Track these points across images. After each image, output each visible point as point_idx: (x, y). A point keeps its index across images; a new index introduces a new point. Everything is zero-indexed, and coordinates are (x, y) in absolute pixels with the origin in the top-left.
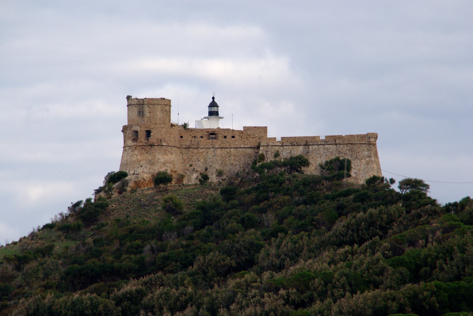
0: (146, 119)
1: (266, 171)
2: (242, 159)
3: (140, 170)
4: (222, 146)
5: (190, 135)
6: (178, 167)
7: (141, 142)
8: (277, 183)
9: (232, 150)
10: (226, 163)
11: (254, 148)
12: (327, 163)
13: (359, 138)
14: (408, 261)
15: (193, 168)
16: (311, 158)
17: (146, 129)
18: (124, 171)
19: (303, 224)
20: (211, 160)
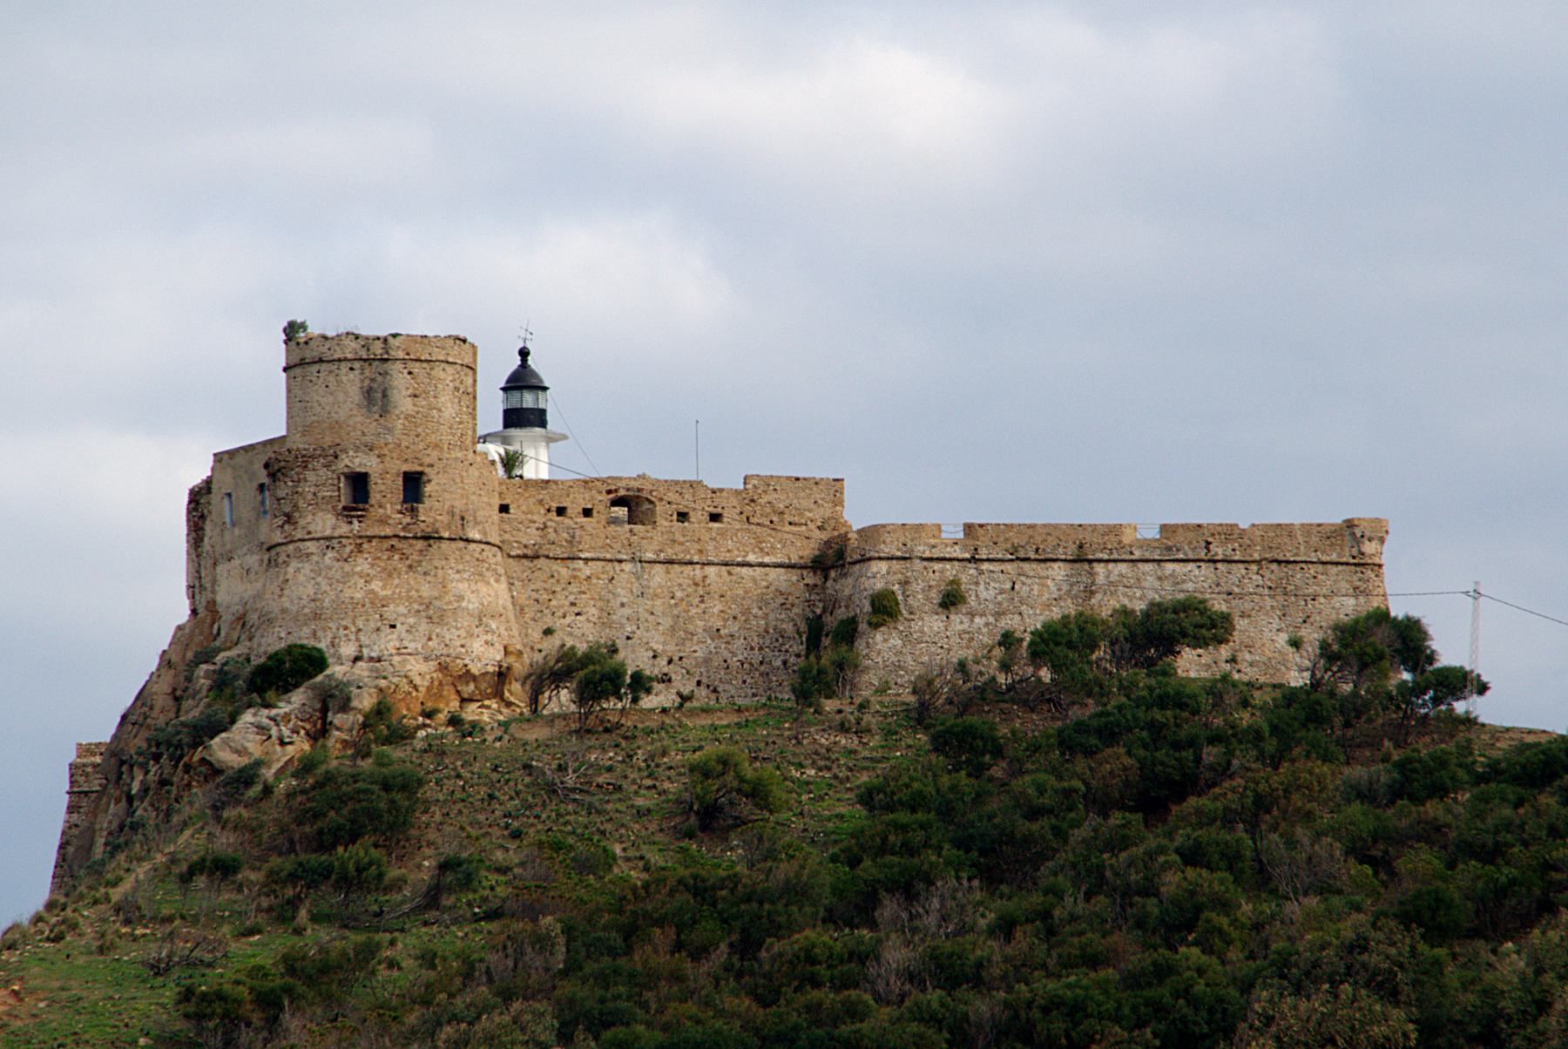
0: (399, 424)
2: (755, 611)
3: (387, 643)
4: (669, 553)
5: (541, 502)
7: (383, 521)
9: (711, 570)
10: (691, 628)
11: (802, 567)
13: (1314, 539)
17: (406, 468)
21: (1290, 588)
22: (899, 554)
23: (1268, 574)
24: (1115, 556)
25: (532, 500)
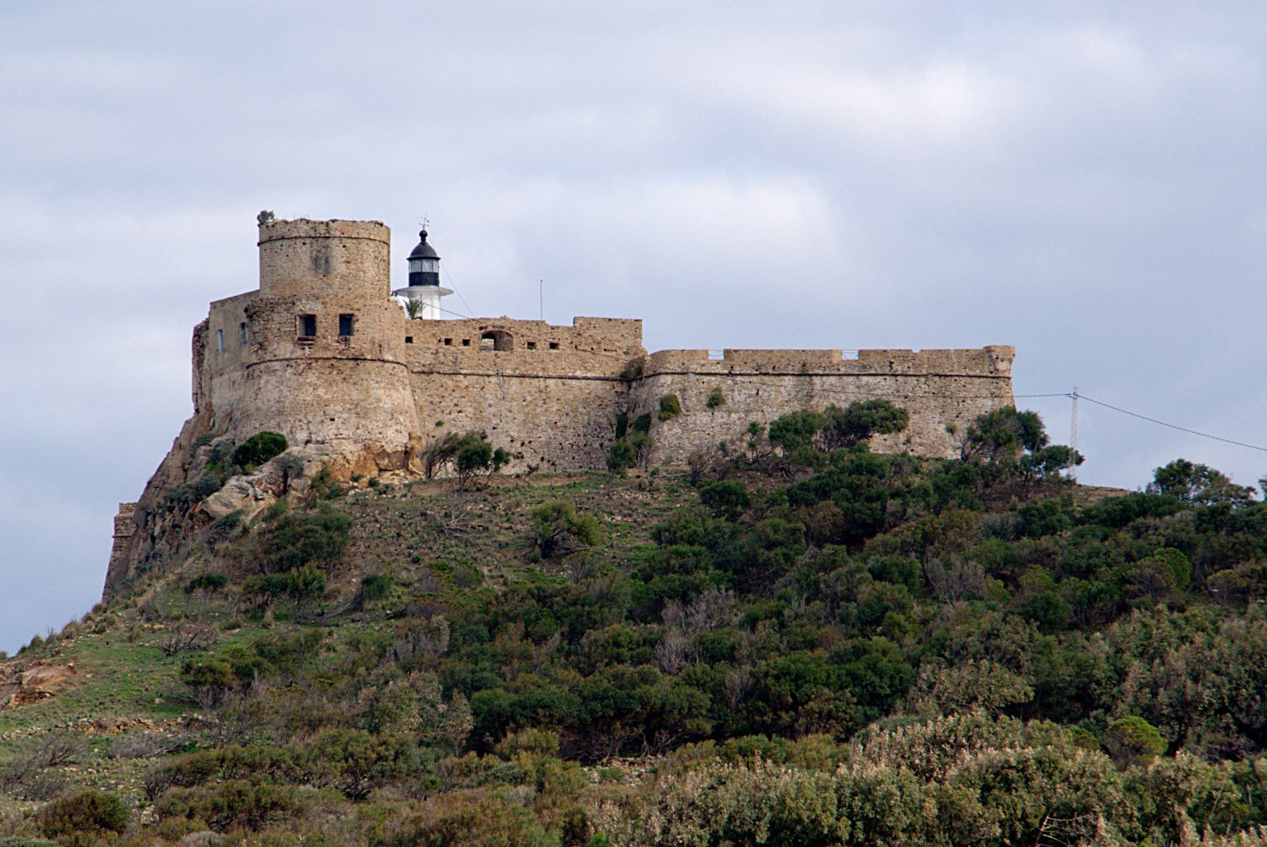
3: (329, 431)
4: (522, 370)
5: (434, 335)
9: (551, 382)
10: (537, 421)
17: (341, 311)
20: (493, 410)
23: (932, 385)
24: (827, 372)
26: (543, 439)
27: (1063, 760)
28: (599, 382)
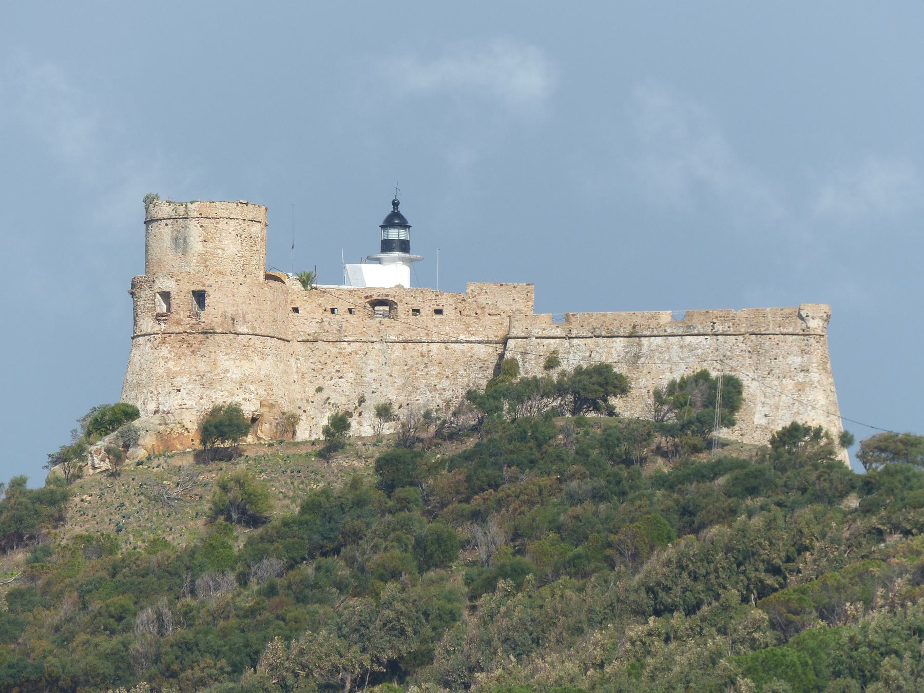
0: (194, 260)
1: (506, 406)
2: (462, 372)
4: (407, 336)
6: (281, 393)
8: (532, 442)
9: (434, 347)
12: (672, 386)
14: (795, 659)
15: (324, 395)
16: (645, 371)
17: (194, 288)
18: (130, 403)
19: (578, 557)
20: (374, 375)
21: (761, 351)
22: (523, 335)
23: (749, 343)
24: (655, 333)
25: (314, 305)
26: (421, 401)
27: (670, 675)
28: (483, 345)
